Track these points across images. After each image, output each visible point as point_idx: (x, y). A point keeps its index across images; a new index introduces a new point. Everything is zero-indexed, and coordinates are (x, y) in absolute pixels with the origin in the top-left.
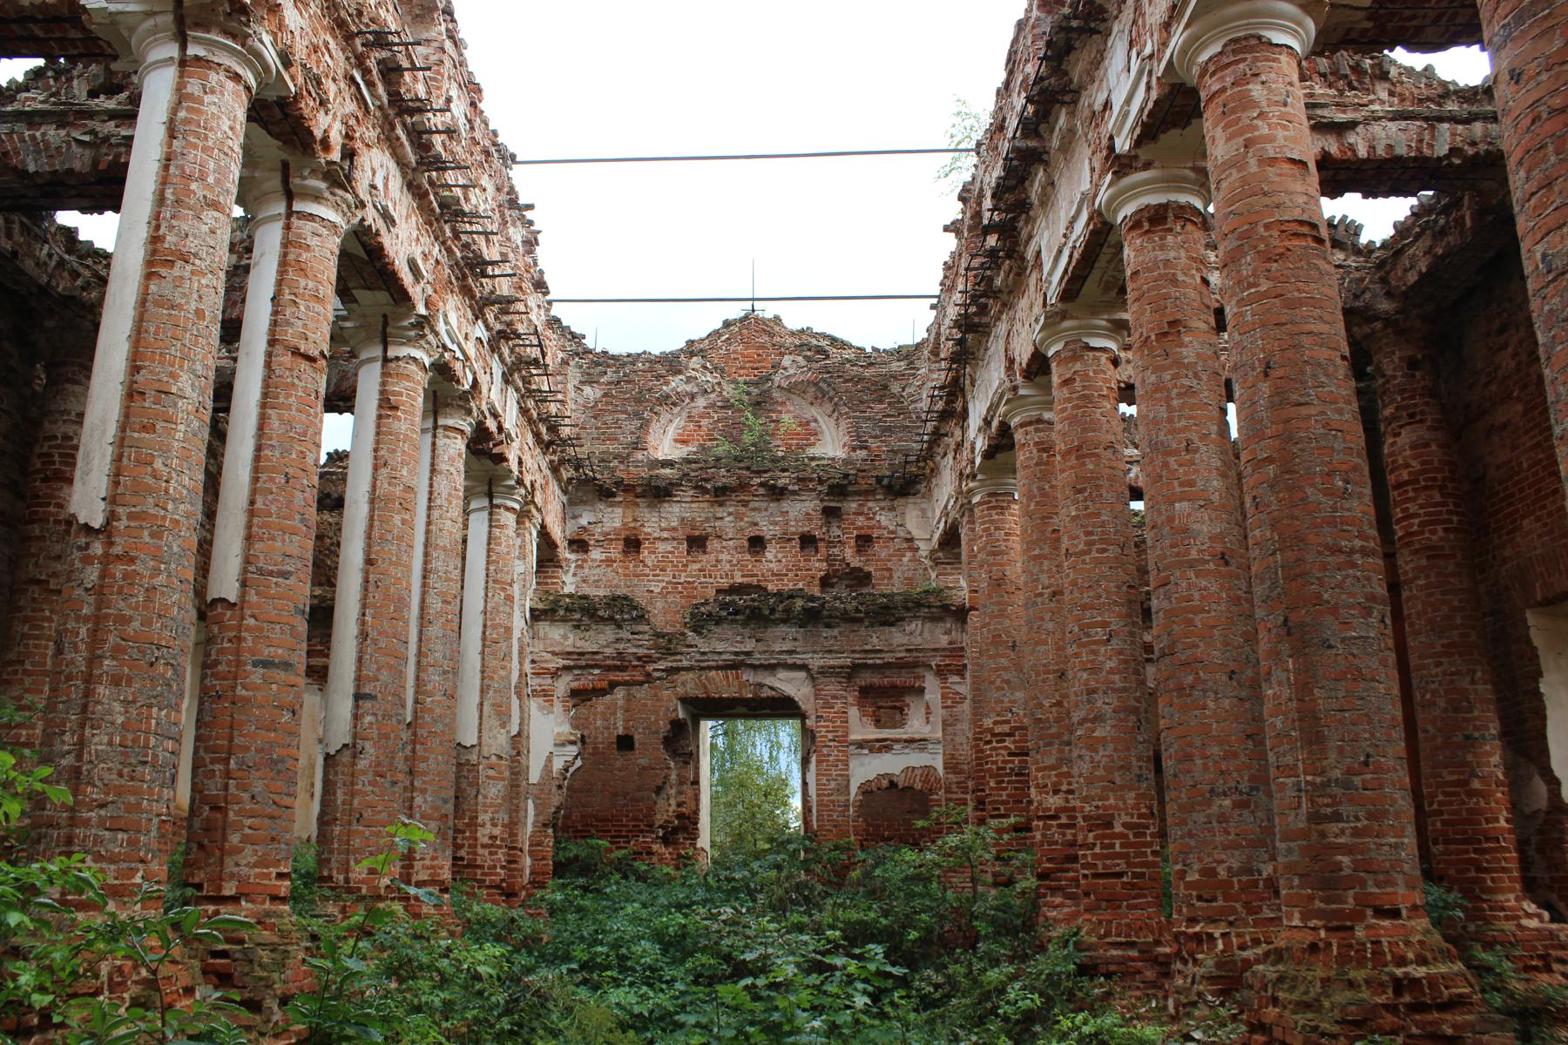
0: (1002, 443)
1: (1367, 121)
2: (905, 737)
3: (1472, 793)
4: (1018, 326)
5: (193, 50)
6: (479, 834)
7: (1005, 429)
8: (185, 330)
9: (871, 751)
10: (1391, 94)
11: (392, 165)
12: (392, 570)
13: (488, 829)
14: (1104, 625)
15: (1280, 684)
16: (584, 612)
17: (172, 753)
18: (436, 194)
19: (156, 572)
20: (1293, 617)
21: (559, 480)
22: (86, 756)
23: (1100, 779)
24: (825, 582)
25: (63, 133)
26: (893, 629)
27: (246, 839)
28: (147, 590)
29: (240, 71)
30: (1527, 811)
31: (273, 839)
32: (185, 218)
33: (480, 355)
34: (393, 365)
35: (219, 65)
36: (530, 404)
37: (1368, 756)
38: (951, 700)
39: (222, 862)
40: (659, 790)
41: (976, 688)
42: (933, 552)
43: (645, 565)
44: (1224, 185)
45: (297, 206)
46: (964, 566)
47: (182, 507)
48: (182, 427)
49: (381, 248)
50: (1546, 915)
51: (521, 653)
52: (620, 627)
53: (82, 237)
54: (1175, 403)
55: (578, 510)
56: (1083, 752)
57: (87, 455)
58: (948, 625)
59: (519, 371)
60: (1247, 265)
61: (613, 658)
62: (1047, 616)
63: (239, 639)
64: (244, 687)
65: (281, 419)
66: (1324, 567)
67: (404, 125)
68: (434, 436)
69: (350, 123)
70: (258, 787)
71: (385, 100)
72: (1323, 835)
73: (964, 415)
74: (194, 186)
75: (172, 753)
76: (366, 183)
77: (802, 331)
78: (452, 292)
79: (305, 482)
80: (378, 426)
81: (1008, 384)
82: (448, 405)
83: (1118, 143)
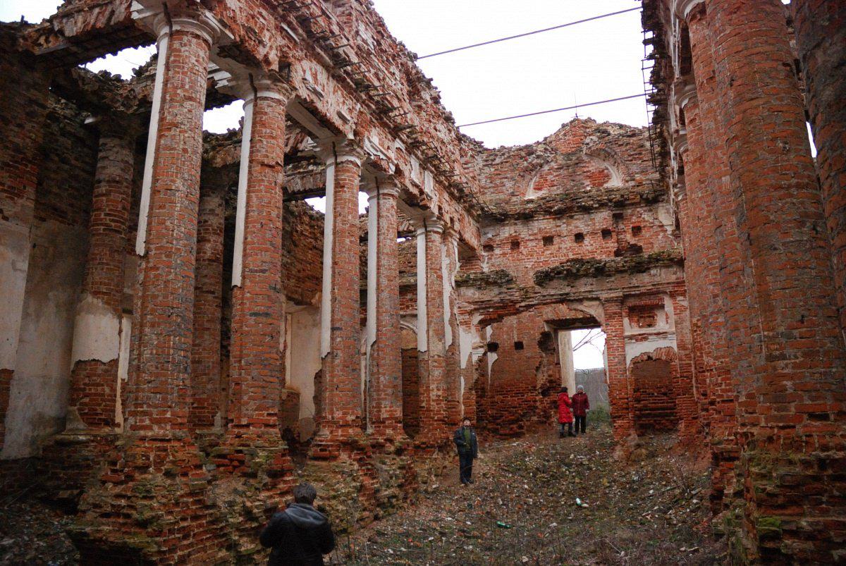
2: (655, 332)
6: (431, 395)
9: (637, 340)
11: (319, 68)
12: (346, 266)
16: (485, 282)
17: (184, 357)
18: (352, 79)
20: (753, 233)
22: (142, 360)
24: (617, 253)
26: (644, 274)
28: (165, 282)
29: (199, 33)
31: (264, 397)
32: (175, 107)
34: (340, 166)
35: (188, 32)
37: (803, 316)
38: (679, 310)
40: (537, 369)
43: (522, 254)
45: (259, 95)
47: (181, 242)
48: (179, 205)
49: (317, 109)
52: (501, 286)
55: (487, 230)
56: (713, 331)
58: (675, 269)
59: (430, 163)
61: (499, 303)
63: (242, 304)
64: (246, 327)
65: (257, 196)
68: (378, 199)
69: (284, 50)
70: (255, 373)
71: (305, 36)
72: (775, 368)
74: (179, 91)
75: (184, 357)
78: (375, 127)
79: (272, 226)
82: (383, 183)
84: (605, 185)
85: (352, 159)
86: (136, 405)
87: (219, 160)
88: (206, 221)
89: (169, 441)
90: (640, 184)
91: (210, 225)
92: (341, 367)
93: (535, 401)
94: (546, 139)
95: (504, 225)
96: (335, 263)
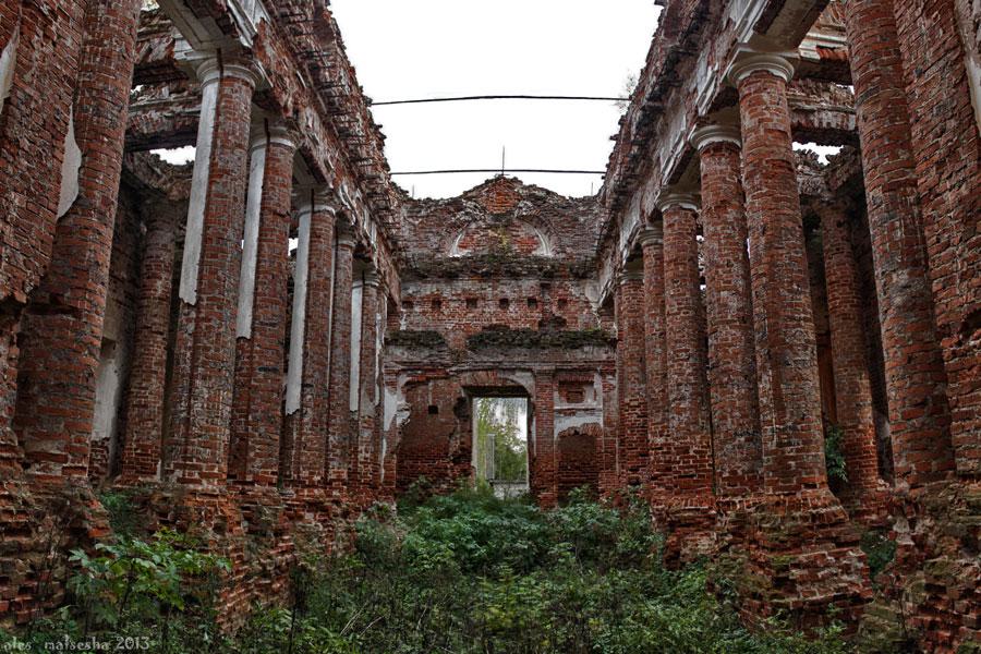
0: (637, 255)
3: (859, 431)
4: (647, 194)
5: (226, 73)
7: (638, 246)
8: (229, 207)
9: (565, 414)
10: (830, 98)
12: (320, 321)
13: (363, 454)
14: (686, 351)
15: (766, 382)
16: (414, 340)
19: (220, 326)
21: (397, 270)
23: (684, 429)
24: (541, 324)
25: (158, 113)
27: (257, 455)
30: (882, 438)
33: (359, 207)
36: (383, 230)
38: (608, 388)
39: (245, 465)
40: (451, 435)
41: (621, 381)
42: (599, 309)
46: (616, 318)
49: (312, 156)
50: (888, 484)
51: (380, 361)
53: (162, 159)
54: (722, 241)
55: (407, 285)
59: (379, 215)
60: (757, 179)
62: (658, 345)
63: (250, 357)
65: (269, 246)
66: (787, 327)
67: (321, 94)
68: (337, 250)
70: (262, 430)
71: (312, 83)
72: (783, 452)
73: (618, 237)
76: (304, 125)
77: (531, 186)
82: (343, 233)
83: (700, 110)
84: (534, 253)
85: (330, 209)
86: (185, 459)
87: (175, 193)
88: (158, 257)
89: (216, 496)
90: (570, 257)
92: (310, 426)
93: (446, 468)
95: (425, 282)
96: (308, 316)
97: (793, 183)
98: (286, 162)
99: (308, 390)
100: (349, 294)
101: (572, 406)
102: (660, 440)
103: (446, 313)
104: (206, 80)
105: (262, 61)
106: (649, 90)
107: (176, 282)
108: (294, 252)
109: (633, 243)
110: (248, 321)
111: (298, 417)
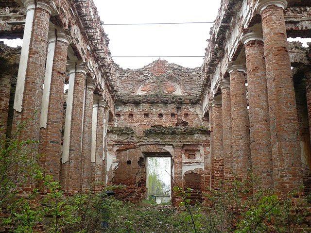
0: (219, 93)
1: (302, 21)
7: (219, 89)
11: (78, 28)
14: (241, 135)
16: (120, 132)
21: (113, 100)
24: (177, 125)
33: (96, 71)
36: (107, 82)
38: (206, 153)
41: (213, 149)
42: (203, 118)
44: (266, 38)
53: (5, 43)
57: (17, 96)
59: (105, 75)
63: (46, 136)
72: (283, 180)
73: (210, 85)
80: (74, 88)
81: (220, 79)
83: (245, 26)
84: (173, 93)
90: (189, 95)
91: (5, 93)
94: (145, 67)
97: (287, 57)
98: (65, 49)
99: (73, 152)
100: (92, 110)
101: (190, 161)
102: (229, 176)
103: (135, 119)
104: (28, 9)
105: (55, 2)
106: (222, 18)
107: (12, 102)
108: (67, 91)
109: (217, 88)
110: (46, 120)
111: (67, 164)
